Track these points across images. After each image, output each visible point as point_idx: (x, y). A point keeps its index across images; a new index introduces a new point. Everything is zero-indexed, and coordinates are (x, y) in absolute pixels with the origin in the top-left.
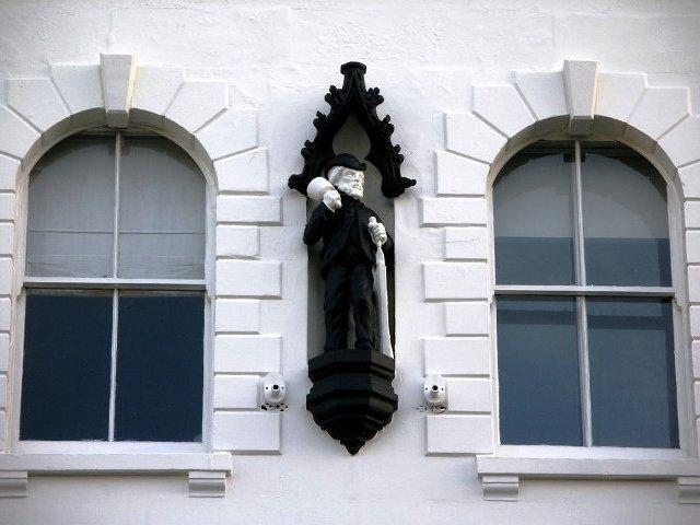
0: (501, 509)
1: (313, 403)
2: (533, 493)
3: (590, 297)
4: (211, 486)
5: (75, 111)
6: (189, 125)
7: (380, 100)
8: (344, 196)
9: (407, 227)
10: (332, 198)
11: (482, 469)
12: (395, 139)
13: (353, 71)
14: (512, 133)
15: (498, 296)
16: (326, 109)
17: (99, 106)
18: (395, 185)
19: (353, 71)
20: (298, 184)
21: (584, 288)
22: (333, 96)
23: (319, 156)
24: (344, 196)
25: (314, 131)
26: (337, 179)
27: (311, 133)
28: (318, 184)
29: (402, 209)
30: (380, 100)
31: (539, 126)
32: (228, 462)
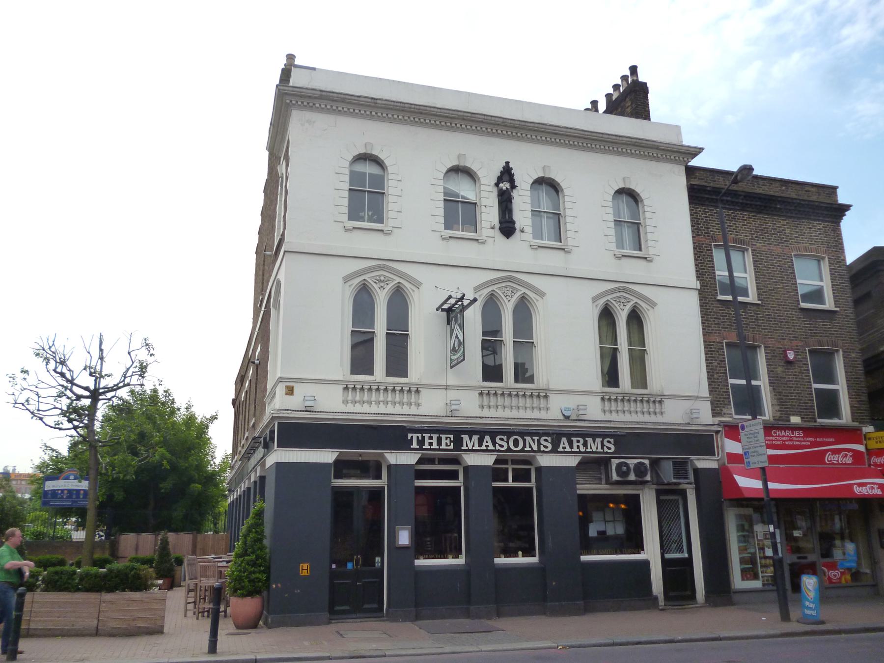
0: (348, 234)
1: (500, 229)
2: (355, 231)
3: (369, 192)
4: (389, 233)
5: (454, 165)
6: (559, 181)
7: (512, 169)
8: (507, 188)
9: (515, 194)
10: (504, 188)
11: (532, 244)
12: (514, 177)
13: (507, 163)
14: (448, 167)
15: (445, 200)
16: (502, 170)
17: (543, 176)
18: (513, 187)
19: (507, 163)
20: (497, 185)
21: (367, 189)
22: (504, 168)
23: (500, 180)
24: (507, 188)
25: (500, 174)
26: (505, 184)
27: (499, 174)
28: (501, 185)
29: (514, 191)
30: (512, 169)
31: (453, 166)
32: (485, 238)
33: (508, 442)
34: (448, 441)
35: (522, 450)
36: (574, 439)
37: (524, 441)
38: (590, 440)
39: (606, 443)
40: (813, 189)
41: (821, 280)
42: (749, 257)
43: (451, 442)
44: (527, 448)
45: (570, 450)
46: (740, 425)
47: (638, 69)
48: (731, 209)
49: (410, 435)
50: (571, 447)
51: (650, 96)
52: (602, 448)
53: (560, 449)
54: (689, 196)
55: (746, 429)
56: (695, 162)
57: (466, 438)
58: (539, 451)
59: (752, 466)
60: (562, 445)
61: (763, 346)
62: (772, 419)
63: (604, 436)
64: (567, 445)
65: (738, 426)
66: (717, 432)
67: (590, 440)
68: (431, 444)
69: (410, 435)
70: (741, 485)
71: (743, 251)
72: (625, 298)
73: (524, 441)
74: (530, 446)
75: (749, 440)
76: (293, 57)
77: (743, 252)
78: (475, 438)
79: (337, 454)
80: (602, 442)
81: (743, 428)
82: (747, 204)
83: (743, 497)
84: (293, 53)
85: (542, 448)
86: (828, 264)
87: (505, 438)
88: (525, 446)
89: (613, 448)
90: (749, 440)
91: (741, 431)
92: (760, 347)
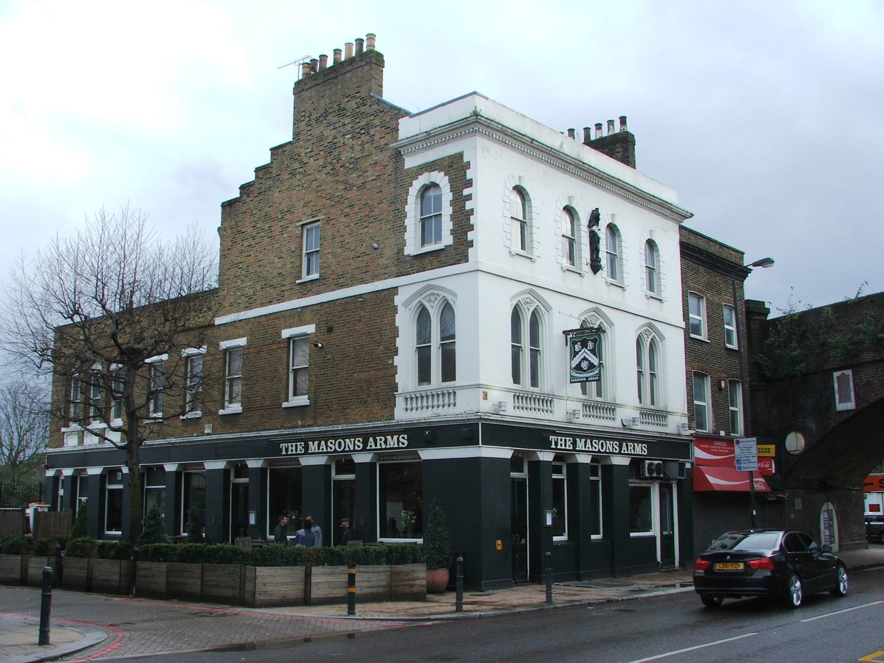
33: (335, 445)
34: (301, 447)
35: (343, 451)
36: (378, 438)
37: (345, 442)
38: (389, 438)
39: (401, 439)
40: (734, 253)
41: (699, 315)
42: (703, 305)
43: (303, 447)
44: (347, 449)
45: (375, 448)
46: (735, 440)
47: (627, 120)
48: (696, 264)
49: (281, 445)
50: (376, 446)
51: (636, 147)
52: (398, 444)
53: (368, 448)
54: (680, 251)
55: (741, 444)
56: (687, 223)
57: (311, 443)
58: (354, 450)
59: (743, 470)
60: (369, 444)
61: (709, 377)
62: (712, 432)
63: (399, 433)
64: (373, 444)
65: (733, 441)
66: (691, 441)
67: (389, 438)
68: (292, 450)
69: (281, 445)
70: (711, 481)
71: (699, 298)
72: (434, 294)
73: (345, 442)
74: (349, 447)
75: (742, 452)
76: (373, 37)
77: (699, 299)
78: (316, 443)
79: (102, 469)
80: (398, 438)
81: (738, 442)
82: (705, 261)
83: (712, 490)
84: (372, 33)
85: (356, 448)
86: (705, 304)
87: (333, 441)
88: (345, 447)
89: (406, 442)
90: (742, 452)
91: (735, 444)
92: (708, 375)
